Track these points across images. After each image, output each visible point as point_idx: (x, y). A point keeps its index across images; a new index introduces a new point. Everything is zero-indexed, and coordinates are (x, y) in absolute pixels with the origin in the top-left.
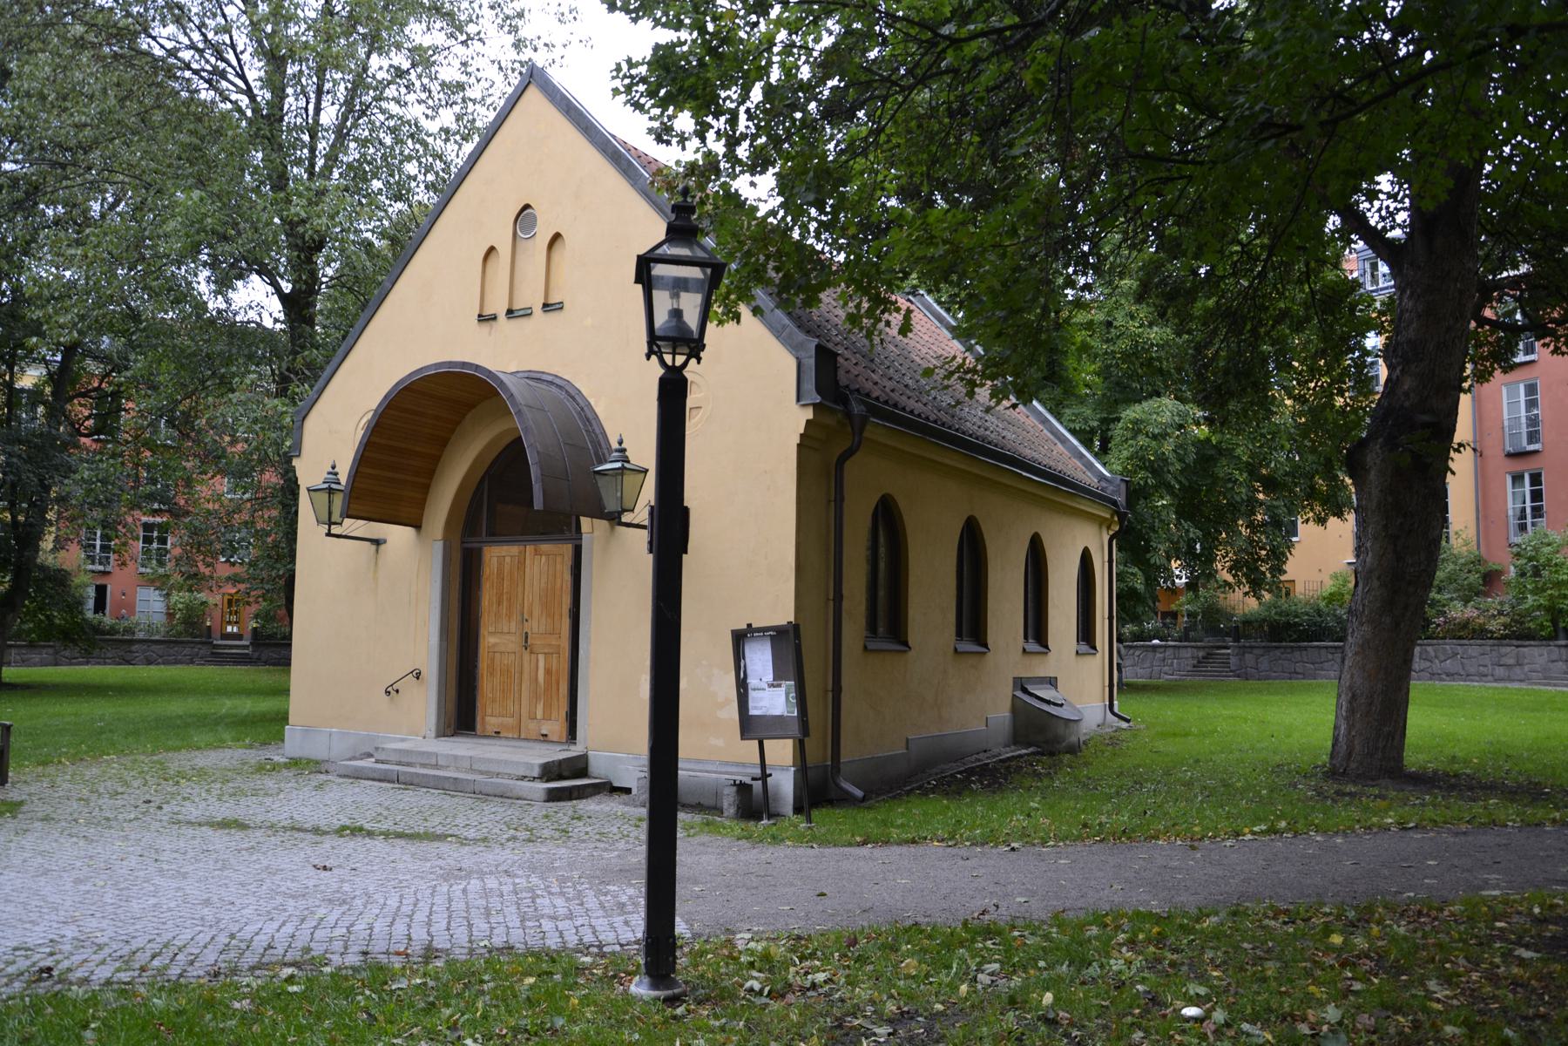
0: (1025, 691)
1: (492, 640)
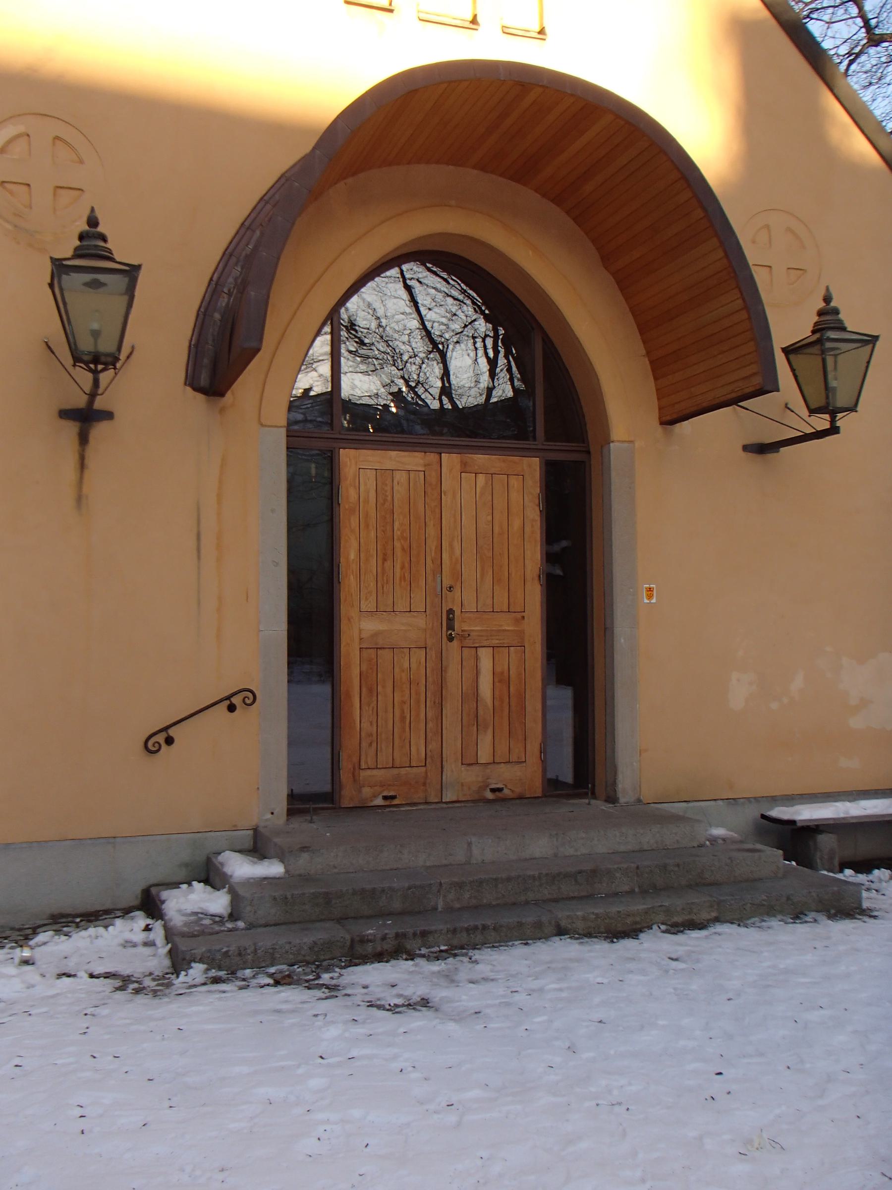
1: (369, 626)
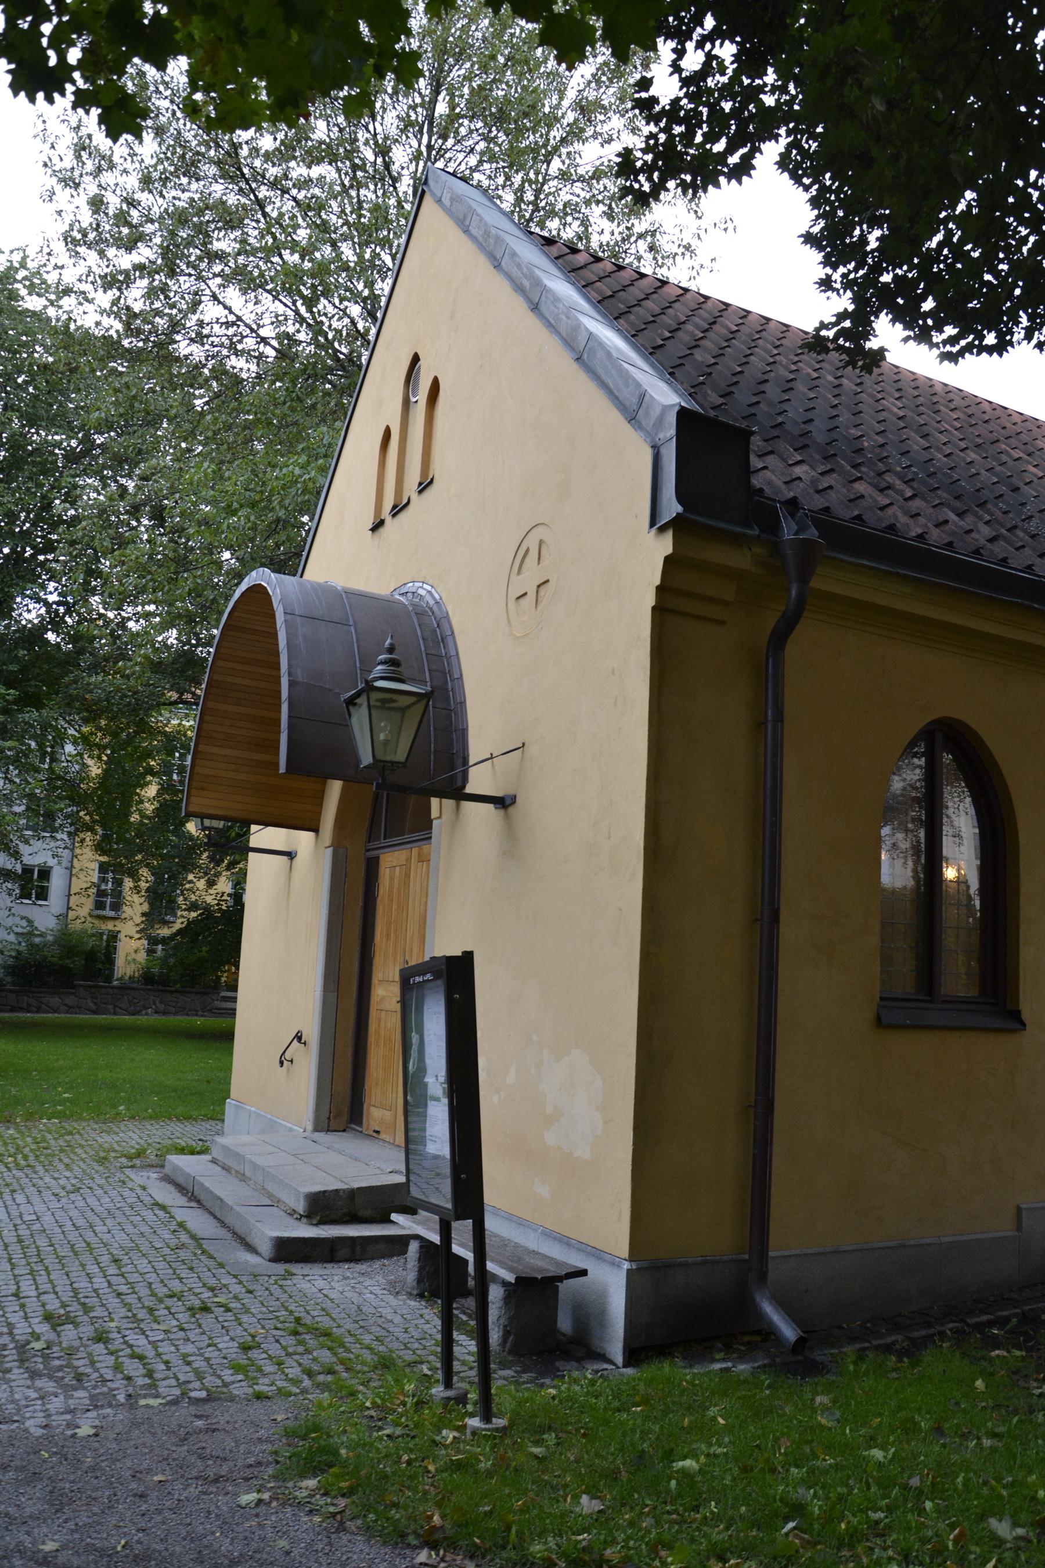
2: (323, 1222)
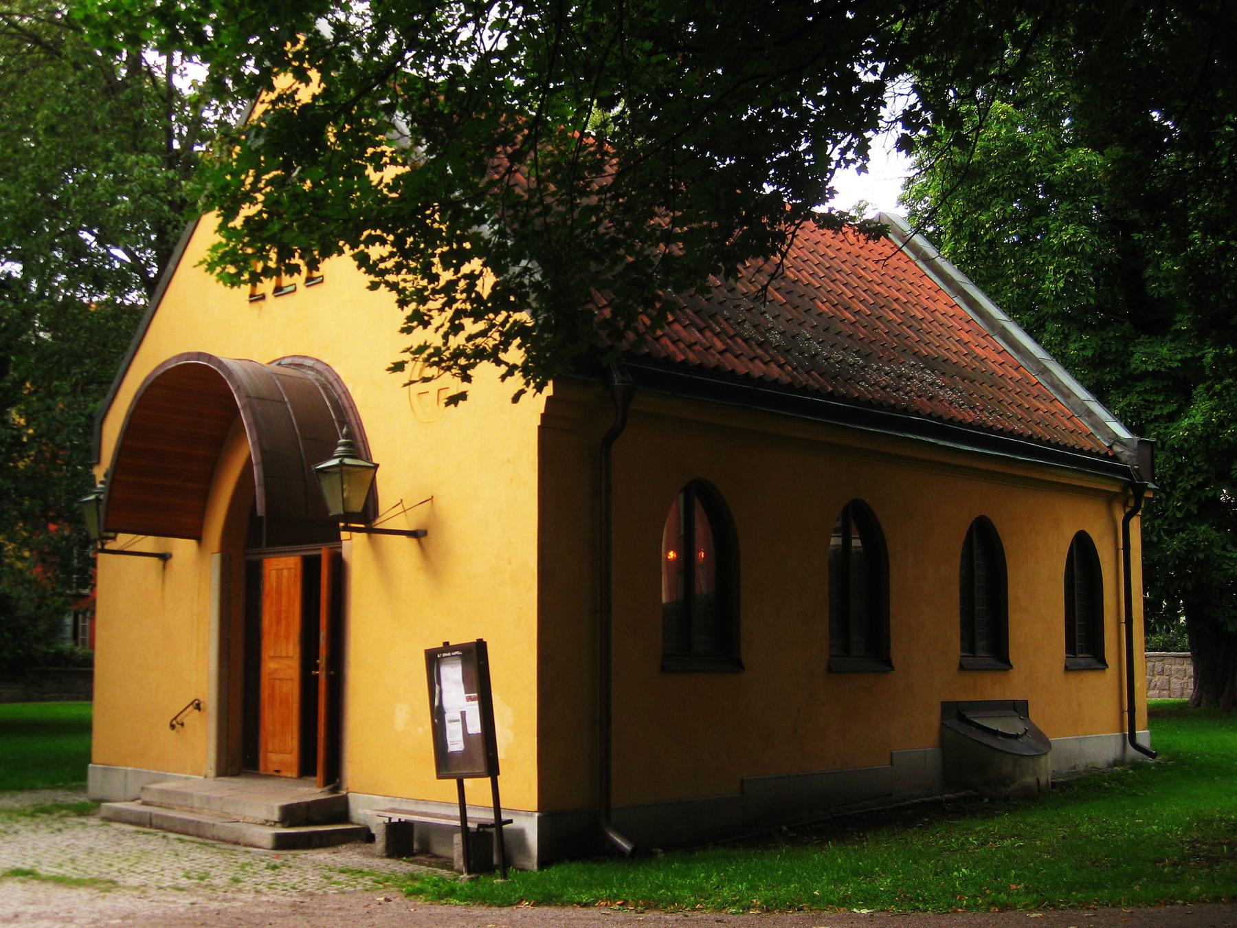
0: (963, 719)
2: (290, 826)
